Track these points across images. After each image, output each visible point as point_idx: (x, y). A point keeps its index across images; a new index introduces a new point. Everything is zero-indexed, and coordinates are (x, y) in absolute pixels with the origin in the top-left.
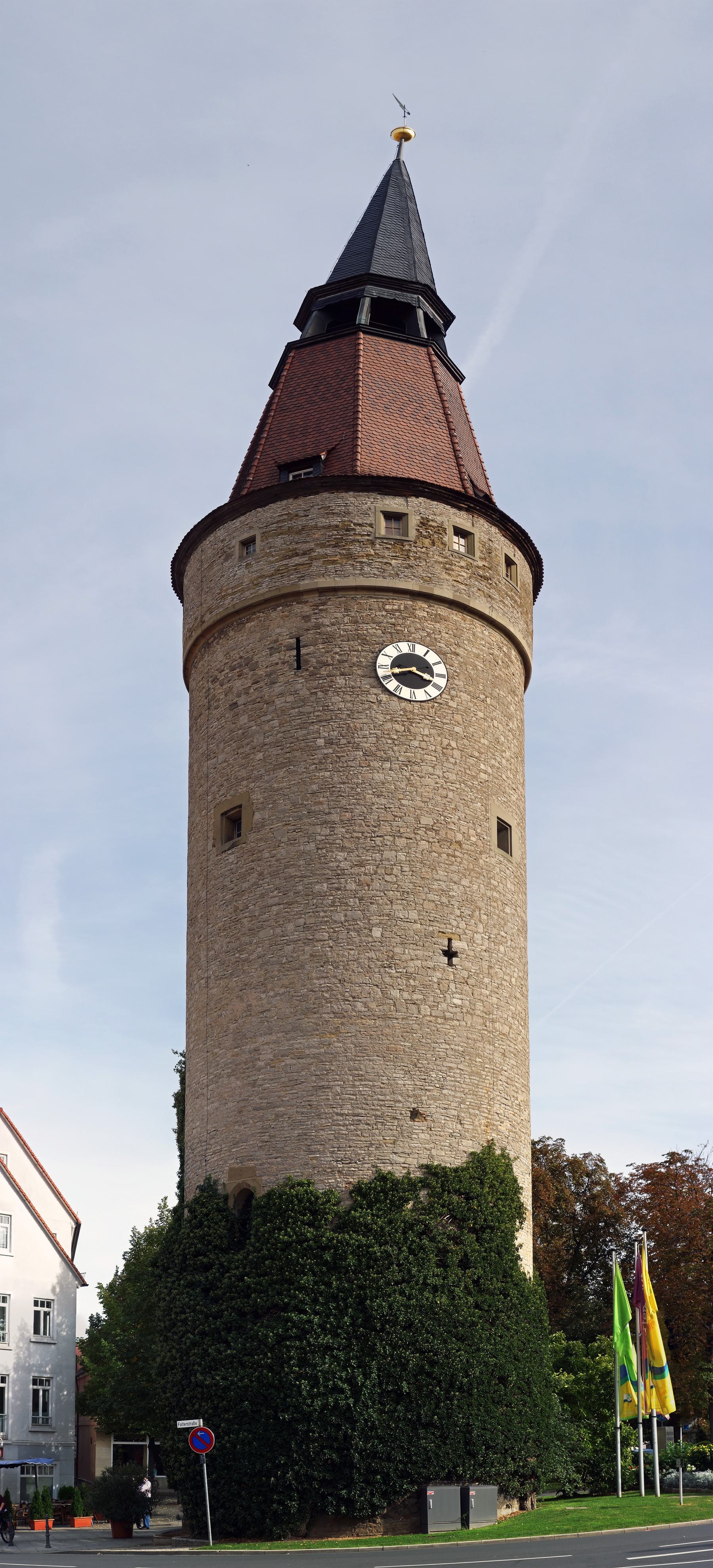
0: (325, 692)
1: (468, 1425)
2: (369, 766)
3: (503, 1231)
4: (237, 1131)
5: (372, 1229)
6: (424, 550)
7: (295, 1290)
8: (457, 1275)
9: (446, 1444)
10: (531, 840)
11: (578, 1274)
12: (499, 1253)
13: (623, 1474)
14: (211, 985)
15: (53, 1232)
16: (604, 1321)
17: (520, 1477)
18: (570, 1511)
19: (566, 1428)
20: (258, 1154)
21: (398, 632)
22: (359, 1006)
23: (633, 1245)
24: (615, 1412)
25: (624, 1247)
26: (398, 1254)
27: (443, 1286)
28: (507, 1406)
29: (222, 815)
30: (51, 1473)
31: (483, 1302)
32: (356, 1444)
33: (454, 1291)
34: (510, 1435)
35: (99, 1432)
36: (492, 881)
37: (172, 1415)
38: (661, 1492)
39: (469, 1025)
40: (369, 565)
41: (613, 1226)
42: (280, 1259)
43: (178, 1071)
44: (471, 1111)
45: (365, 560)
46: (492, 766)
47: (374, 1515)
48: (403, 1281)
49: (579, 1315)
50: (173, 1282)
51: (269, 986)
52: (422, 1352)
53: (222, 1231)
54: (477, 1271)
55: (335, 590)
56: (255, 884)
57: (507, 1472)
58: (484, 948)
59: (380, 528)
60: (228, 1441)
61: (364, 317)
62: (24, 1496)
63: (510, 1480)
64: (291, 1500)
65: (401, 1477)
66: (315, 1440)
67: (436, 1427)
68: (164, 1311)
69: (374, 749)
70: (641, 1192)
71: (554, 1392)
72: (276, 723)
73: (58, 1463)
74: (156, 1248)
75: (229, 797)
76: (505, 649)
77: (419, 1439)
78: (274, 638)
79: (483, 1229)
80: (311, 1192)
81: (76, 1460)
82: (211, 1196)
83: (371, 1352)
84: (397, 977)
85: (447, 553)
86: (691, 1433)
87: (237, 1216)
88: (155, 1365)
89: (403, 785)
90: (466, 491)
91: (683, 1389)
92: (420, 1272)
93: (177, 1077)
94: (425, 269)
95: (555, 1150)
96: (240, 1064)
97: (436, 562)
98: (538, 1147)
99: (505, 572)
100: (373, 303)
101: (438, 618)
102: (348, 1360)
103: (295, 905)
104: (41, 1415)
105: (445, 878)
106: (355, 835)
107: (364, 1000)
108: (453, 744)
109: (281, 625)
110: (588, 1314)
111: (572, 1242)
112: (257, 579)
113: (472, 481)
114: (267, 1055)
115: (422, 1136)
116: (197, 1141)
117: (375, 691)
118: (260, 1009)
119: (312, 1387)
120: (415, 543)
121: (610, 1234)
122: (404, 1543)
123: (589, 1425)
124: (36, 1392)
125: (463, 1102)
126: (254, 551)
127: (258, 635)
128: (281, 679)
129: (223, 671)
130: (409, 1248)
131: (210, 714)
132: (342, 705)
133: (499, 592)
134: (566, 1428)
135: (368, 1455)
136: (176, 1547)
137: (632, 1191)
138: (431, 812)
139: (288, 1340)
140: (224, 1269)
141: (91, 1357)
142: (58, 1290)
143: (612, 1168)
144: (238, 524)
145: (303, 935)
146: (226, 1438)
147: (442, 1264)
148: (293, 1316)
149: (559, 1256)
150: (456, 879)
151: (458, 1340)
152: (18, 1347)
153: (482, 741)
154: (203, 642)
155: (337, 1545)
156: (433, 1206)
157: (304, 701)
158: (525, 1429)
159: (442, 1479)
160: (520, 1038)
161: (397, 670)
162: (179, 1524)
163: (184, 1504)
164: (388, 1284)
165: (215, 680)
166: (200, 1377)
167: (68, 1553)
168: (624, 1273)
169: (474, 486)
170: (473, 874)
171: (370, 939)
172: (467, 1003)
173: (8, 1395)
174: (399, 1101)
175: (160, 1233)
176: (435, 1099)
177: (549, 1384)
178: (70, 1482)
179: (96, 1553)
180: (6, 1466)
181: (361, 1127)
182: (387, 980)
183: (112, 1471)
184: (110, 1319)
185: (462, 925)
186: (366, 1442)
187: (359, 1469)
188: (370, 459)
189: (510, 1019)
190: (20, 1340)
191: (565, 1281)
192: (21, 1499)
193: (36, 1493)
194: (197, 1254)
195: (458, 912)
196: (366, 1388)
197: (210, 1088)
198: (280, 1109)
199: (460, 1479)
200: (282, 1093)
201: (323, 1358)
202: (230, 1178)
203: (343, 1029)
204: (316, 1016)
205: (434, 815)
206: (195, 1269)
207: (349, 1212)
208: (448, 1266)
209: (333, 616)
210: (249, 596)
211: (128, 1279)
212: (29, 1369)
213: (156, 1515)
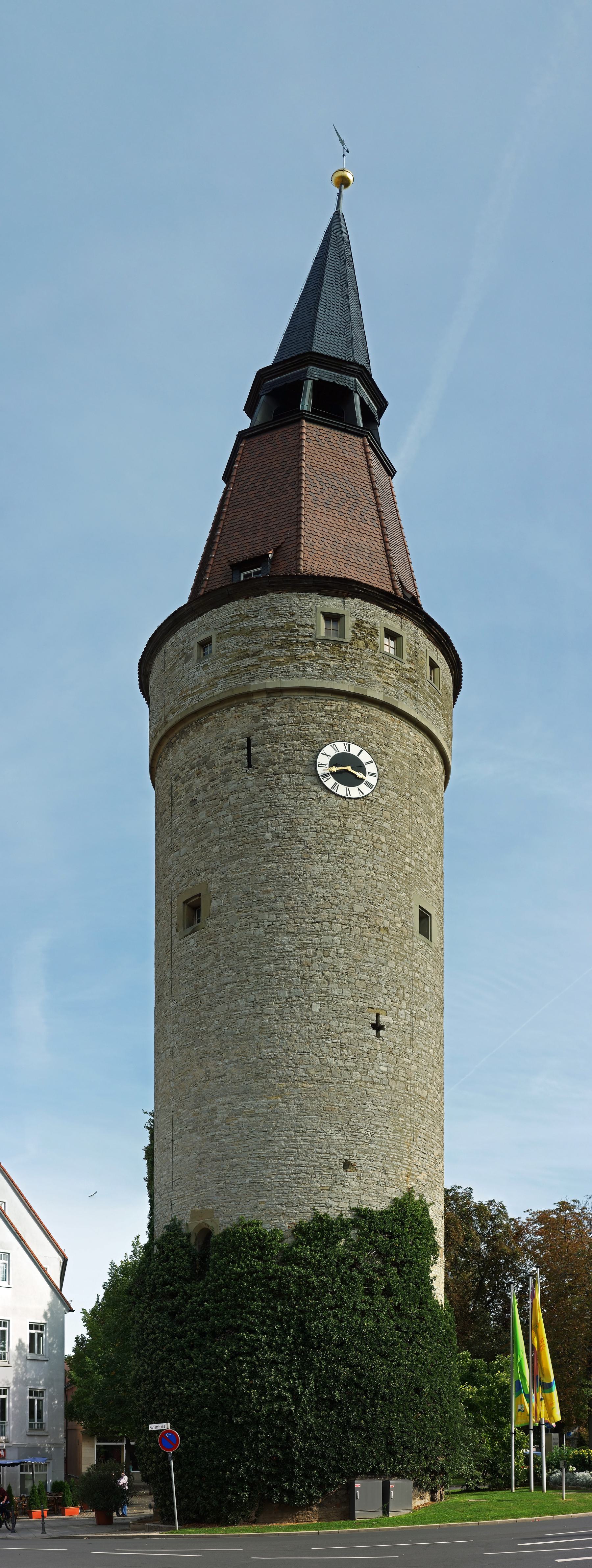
0: (272, 789)
1: (389, 1428)
2: (310, 858)
3: (420, 1265)
4: (198, 1179)
5: (310, 1262)
6: (358, 652)
7: (246, 1313)
8: (381, 1302)
9: (370, 1444)
10: (448, 928)
11: (482, 1303)
12: (416, 1284)
13: (516, 1472)
14: (175, 1054)
16: (502, 1343)
17: (432, 1473)
18: (472, 1503)
19: (470, 1433)
20: (215, 1198)
21: (335, 732)
22: (301, 1072)
23: (528, 1279)
24: (511, 1420)
25: (521, 1280)
26: (333, 1284)
27: (369, 1311)
28: (421, 1413)
29: (184, 903)
30: (46, 1470)
31: (403, 1325)
32: (297, 1444)
33: (378, 1315)
34: (423, 1437)
35: (85, 1435)
36: (415, 963)
37: (145, 1419)
40: (311, 666)
41: (512, 1263)
42: (234, 1288)
43: (148, 1128)
44: (394, 1163)
45: (307, 661)
46: (416, 860)
47: (311, 1504)
48: (336, 1306)
49: (483, 1337)
51: (225, 1054)
52: (351, 1366)
54: (398, 1299)
55: (281, 691)
56: (213, 965)
59: (320, 630)
60: (191, 1442)
61: (306, 403)
62: (23, 1490)
65: (334, 1472)
67: (363, 1430)
68: (137, 1332)
69: (314, 842)
70: (536, 1234)
72: (230, 818)
73: (51, 1461)
74: (130, 1279)
75: (190, 887)
76: (428, 750)
77: (349, 1439)
78: (228, 737)
79: (403, 1263)
80: (260, 1231)
81: (66, 1459)
83: (310, 1366)
84: (333, 1047)
85: (378, 655)
86: (573, 1439)
88: (131, 1378)
89: (339, 876)
90: (396, 593)
93: (147, 1133)
94: (361, 347)
95: (465, 1197)
96: (200, 1122)
97: (369, 664)
98: (451, 1194)
99: (429, 675)
100: (313, 390)
101: (370, 719)
102: (290, 1373)
103: (247, 984)
104: (36, 1421)
105: (374, 960)
106: (298, 920)
107: (305, 1066)
108: (383, 839)
109: (234, 725)
111: (477, 1276)
113: (401, 583)
114: (222, 1114)
115: (353, 1184)
116: (164, 1187)
117: (315, 788)
118: (217, 1074)
119: (260, 1395)
120: (351, 644)
121: (509, 1270)
122: (336, 1528)
123: (489, 1430)
124: (32, 1402)
125: (388, 1155)
126: (211, 652)
127: (214, 735)
129: (184, 769)
130: (341, 1279)
132: (287, 802)
133: (423, 694)
134: (470, 1433)
136: (149, 1531)
138: (362, 901)
141: (77, 1372)
142: (49, 1315)
145: (253, 1010)
146: (190, 1439)
147: (369, 1292)
148: (245, 1335)
149: (466, 1287)
150: (383, 961)
152: (16, 1364)
153: (408, 836)
154: (166, 741)
155: (280, 1530)
156: (361, 1243)
157: (254, 798)
158: (436, 1432)
159: (367, 1474)
161: (334, 769)
162: (151, 1512)
163: (155, 1495)
164: (324, 1309)
166: (167, 1387)
167: (60, 1538)
168: (521, 1303)
169: (403, 588)
170: (398, 957)
171: (310, 1014)
172: (392, 1070)
173: (9, 1405)
174: (334, 1154)
175: (134, 1266)
176: (364, 1152)
177: (456, 1395)
178: (61, 1477)
179: (83, 1537)
180: (8, 1465)
181: (301, 1176)
182: (325, 1049)
183: (96, 1468)
184: (93, 1339)
185: (389, 1002)
186: (305, 1442)
187: (299, 1465)
188: (313, 559)
189: (428, 1084)
190: (18, 1358)
191: (471, 1308)
192: (21, 1492)
193: (33, 1487)
194: (165, 1283)
195: (385, 991)
196: (305, 1396)
197: (175, 1142)
198: (235, 1160)
199: (382, 1474)
200: (236, 1147)
201: (269, 1371)
202: (192, 1218)
203: (287, 1092)
204: (264, 1080)
205: (365, 904)
207: (291, 1248)
208: (373, 1294)
209: (280, 716)
211: (107, 1306)
212: (26, 1383)
213: (132, 1505)
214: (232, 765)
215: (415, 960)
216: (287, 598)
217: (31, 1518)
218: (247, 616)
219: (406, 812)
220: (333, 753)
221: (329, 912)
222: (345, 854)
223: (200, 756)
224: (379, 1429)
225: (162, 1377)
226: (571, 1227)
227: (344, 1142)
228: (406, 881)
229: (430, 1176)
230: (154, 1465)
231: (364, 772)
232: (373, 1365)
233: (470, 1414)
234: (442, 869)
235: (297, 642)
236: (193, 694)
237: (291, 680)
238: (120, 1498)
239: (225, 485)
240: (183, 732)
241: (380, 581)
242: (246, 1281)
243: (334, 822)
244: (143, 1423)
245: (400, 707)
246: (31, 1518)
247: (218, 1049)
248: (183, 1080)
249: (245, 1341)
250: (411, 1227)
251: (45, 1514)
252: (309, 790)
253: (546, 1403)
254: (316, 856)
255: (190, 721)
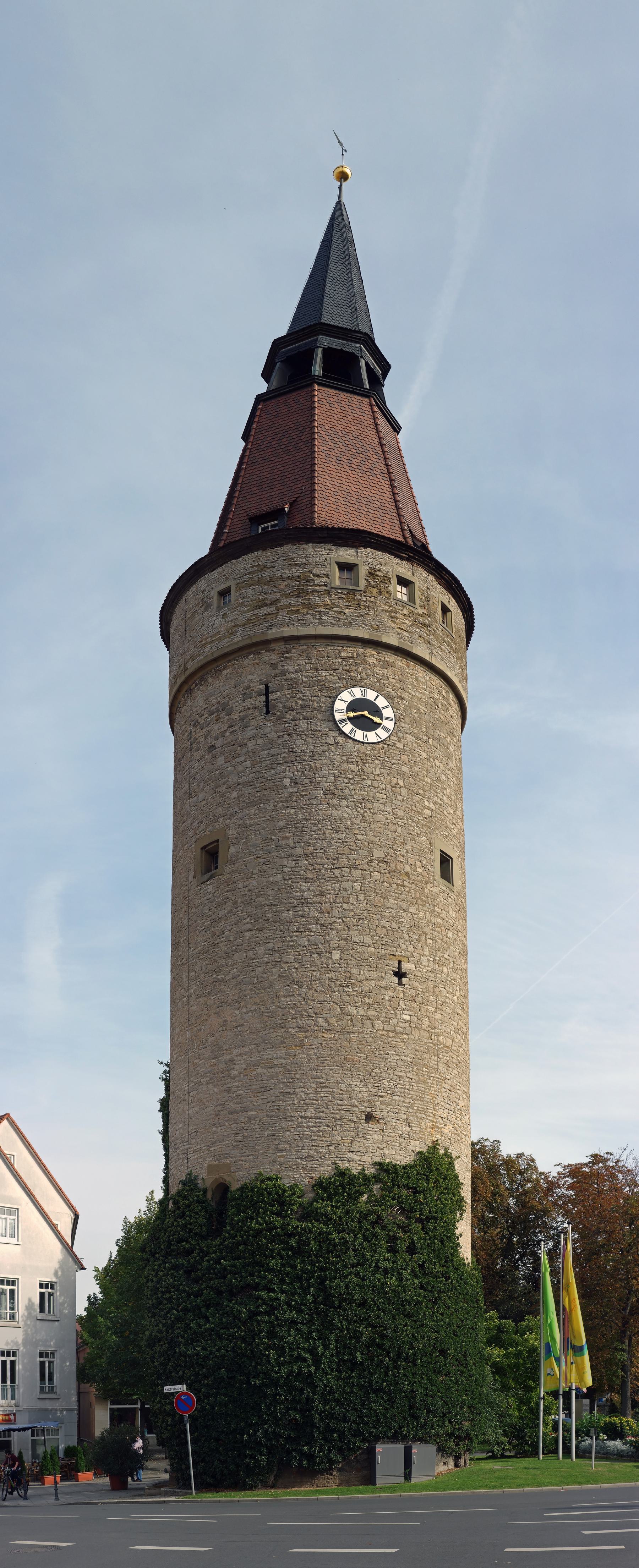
0: (290, 735)
1: (412, 1391)
2: (328, 803)
3: (445, 1222)
4: (215, 1132)
6: (372, 599)
7: (265, 1272)
9: (393, 1407)
10: (472, 872)
11: (510, 1261)
12: (442, 1241)
13: (544, 1439)
14: (192, 1003)
15: (55, 1222)
17: (456, 1438)
18: (498, 1470)
19: (497, 1397)
20: (233, 1152)
21: (352, 678)
23: (559, 1236)
24: (539, 1384)
25: (552, 1238)
26: (354, 1241)
27: (392, 1269)
28: (446, 1375)
29: (202, 849)
30: (58, 1434)
31: (427, 1283)
32: (317, 1406)
34: (448, 1400)
35: (97, 1397)
36: (437, 909)
37: (160, 1381)
38: (577, 1457)
39: (417, 1038)
40: (327, 614)
42: (252, 1245)
43: (163, 1079)
44: (419, 1115)
45: (323, 609)
46: (435, 803)
47: (331, 1469)
48: (358, 1264)
49: (511, 1297)
50: (160, 1265)
51: (243, 1003)
52: (373, 1326)
53: (201, 1220)
54: (422, 1257)
56: (231, 911)
57: (445, 1433)
58: (430, 969)
60: (208, 1404)
61: (317, 369)
62: (35, 1455)
63: (447, 1440)
64: (261, 1455)
66: (282, 1403)
67: (385, 1393)
68: (151, 1290)
69: (332, 788)
70: (567, 1189)
71: (487, 1364)
73: (63, 1426)
74: (145, 1236)
75: (208, 833)
77: (370, 1402)
78: (247, 684)
79: (428, 1219)
80: (279, 1186)
82: (192, 1189)
83: (329, 1326)
84: (354, 996)
85: (393, 602)
86: (604, 1405)
87: (215, 1206)
88: (145, 1338)
89: (358, 822)
90: (406, 541)
91: (599, 1366)
92: (372, 1256)
93: (162, 1085)
94: (365, 317)
95: (492, 1150)
96: (217, 1073)
97: (383, 610)
98: (477, 1147)
99: (441, 619)
100: (324, 356)
101: (386, 665)
102: (310, 1333)
103: (265, 931)
105: (395, 906)
106: (317, 867)
107: (325, 1016)
108: (401, 783)
109: (252, 672)
110: (518, 1297)
111: (506, 1233)
112: (231, 628)
113: (410, 531)
114: (240, 1065)
115: (375, 1137)
116: (179, 1141)
117: (333, 733)
118: (235, 1024)
119: (279, 1356)
120: (365, 592)
122: (356, 1493)
123: (517, 1394)
124: (42, 1364)
125: (411, 1107)
126: (230, 601)
127: (233, 682)
128: (253, 723)
130: (364, 1235)
131: (191, 755)
132: (305, 747)
133: (437, 638)
135: (327, 1415)
136: (165, 1496)
137: (559, 1188)
138: (382, 846)
139: (259, 1315)
140: (204, 1254)
141: (89, 1332)
142: (60, 1273)
143: (542, 1167)
144: (216, 575)
145: (272, 958)
146: (206, 1401)
147: (392, 1250)
148: (263, 1294)
149: (494, 1244)
150: (405, 907)
151: (405, 1316)
152: (26, 1324)
153: (426, 779)
154: (186, 688)
155: (299, 1495)
156: (384, 1199)
157: (272, 744)
158: (461, 1396)
159: (389, 1438)
160: (461, 1050)
161: (351, 714)
162: (167, 1476)
163: (171, 1459)
164: (345, 1267)
165: (196, 724)
166: (183, 1348)
167: (73, 1504)
168: (551, 1260)
169: (413, 536)
170: (419, 902)
171: (330, 961)
172: (415, 1019)
174: (356, 1106)
175: (148, 1223)
176: (387, 1104)
177: (482, 1357)
178: (74, 1442)
179: (97, 1503)
180: (19, 1430)
181: (322, 1128)
182: (345, 998)
183: (110, 1431)
185: (411, 948)
186: (325, 1404)
187: (318, 1428)
188: (327, 512)
189: (452, 1033)
191: (499, 1267)
193: (45, 1452)
194: (180, 1240)
195: (407, 937)
196: (326, 1357)
197: (191, 1094)
199: (404, 1438)
200: (254, 1099)
201: (289, 1331)
203: (306, 1042)
204: (283, 1030)
206: (178, 1254)
207: (312, 1204)
208: (397, 1252)
209: (297, 663)
210: (226, 645)
211: (120, 1263)
213: (147, 1469)
214: (251, 711)
215: (437, 905)
216: (303, 550)
217: (43, 1484)
218: (265, 567)
219: (424, 755)
220: (349, 699)
221: (348, 858)
222: (364, 799)
223: (218, 703)
224: (402, 1391)
225: (178, 1337)
226: (605, 1181)
227: (366, 1094)
228: (425, 825)
229: (455, 1129)
230: (169, 1428)
231: (381, 716)
232: (396, 1325)
233: (497, 1377)
234: (462, 811)
235: (313, 591)
236: (213, 642)
237: (307, 628)
238: (135, 1463)
239: (244, 444)
240: (202, 679)
241: (389, 530)
242: (265, 1238)
243: (352, 767)
244: (158, 1385)
245: (414, 651)
246: (43, 1484)
247: (236, 998)
248: (200, 1030)
249: (263, 1300)
250: (436, 1182)
251: (58, 1479)
252: (327, 736)
253: (577, 1367)
254: (334, 802)
255: (209, 668)
